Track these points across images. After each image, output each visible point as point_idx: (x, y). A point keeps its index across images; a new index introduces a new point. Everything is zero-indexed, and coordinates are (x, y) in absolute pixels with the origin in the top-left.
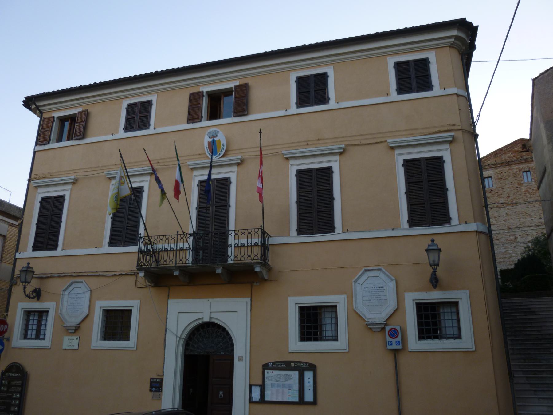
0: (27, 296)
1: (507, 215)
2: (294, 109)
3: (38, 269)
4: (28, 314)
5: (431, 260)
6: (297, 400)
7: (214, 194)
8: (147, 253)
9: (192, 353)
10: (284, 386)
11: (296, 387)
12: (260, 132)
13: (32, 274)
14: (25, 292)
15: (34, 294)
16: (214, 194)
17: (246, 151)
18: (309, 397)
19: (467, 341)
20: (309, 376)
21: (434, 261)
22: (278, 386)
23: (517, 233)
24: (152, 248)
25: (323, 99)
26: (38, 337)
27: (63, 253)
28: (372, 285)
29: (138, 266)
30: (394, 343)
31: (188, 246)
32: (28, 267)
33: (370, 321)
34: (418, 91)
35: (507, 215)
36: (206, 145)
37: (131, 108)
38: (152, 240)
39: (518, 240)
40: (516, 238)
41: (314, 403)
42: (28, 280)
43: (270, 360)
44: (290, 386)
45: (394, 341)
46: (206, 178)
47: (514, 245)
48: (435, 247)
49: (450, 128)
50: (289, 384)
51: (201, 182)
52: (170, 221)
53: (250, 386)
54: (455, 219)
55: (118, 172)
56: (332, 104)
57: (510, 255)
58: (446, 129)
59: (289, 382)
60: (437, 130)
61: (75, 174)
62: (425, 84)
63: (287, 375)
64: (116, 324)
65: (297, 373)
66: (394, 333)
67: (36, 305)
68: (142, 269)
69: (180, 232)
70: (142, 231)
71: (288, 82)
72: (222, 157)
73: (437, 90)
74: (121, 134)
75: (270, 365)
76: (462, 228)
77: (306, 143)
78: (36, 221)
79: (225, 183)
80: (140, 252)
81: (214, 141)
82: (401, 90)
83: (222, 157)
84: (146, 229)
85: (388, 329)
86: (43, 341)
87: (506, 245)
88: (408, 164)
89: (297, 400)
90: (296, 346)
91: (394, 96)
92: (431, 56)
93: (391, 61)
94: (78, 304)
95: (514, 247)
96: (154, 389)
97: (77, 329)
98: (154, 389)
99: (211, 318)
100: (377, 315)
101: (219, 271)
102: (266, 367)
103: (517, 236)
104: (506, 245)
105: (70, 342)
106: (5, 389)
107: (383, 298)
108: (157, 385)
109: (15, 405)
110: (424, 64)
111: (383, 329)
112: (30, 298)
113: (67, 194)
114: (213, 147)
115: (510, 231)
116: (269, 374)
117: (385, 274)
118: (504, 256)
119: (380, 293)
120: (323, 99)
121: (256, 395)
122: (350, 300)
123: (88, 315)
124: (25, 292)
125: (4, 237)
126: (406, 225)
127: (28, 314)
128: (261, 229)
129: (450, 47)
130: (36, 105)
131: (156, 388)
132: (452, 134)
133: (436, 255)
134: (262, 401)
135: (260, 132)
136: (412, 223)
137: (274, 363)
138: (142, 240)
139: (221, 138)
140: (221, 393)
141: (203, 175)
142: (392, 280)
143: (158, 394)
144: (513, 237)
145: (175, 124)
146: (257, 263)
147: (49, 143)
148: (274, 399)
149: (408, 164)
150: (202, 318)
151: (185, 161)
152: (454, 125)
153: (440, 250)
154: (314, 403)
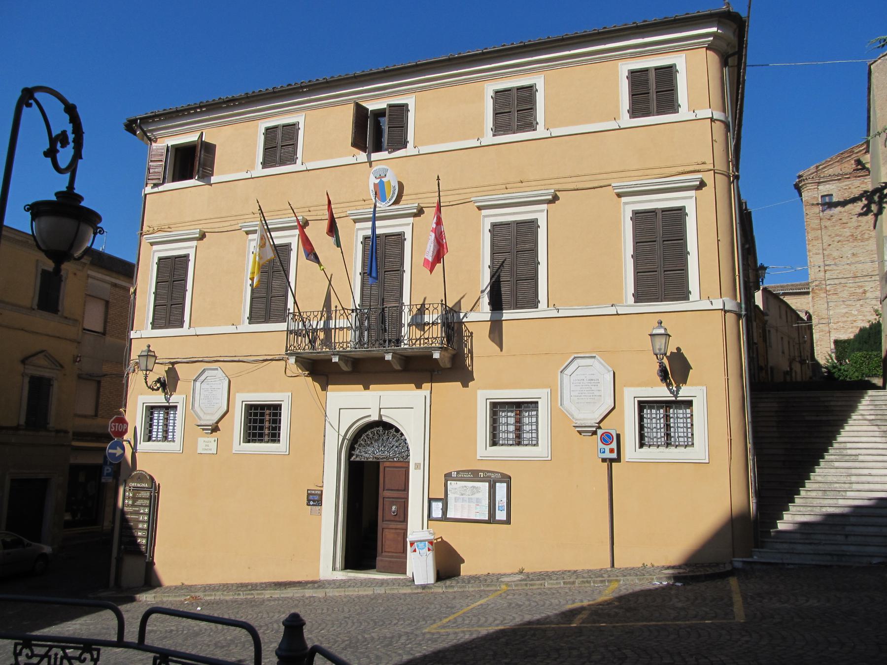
0: (149, 388)
1: (853, 255)
2: (489, 138)
3: (164, 352)
4: (151, 410)
5: (657, 347)
6: (115, 639)
7: (382, 256)
8: (297, 333)
9: (358, 459)
10: (470, 500)
11: (486, 502)
12: (438, 179)
13: (153, 359)
14: (146, 383)
15: (158, 385)
16: (382, 256)
17: (425, 196)
18: (501, 515)
19: (699, 451)
20: (501, 489)
21: (660, 349)
22: (463, 500)
23: (867, 283)
24: (304, 325)
25: (529, 124)
26: (165, 438)
27: (192, 331)
28: (583, 377)
29: (287, 350)
30: (607, 451)
31: (349, 325)
32: (149, 351)
33: (579, 423)
34: (660, 112)
35: (853, 255)
36: (372, 187)
37: (270, 132)
38: (305, 316)
39: (868, 295)
40: (865, 292)
41: (508, 521)
42: (150, 367)
43: (453, 469)
44: (478, 501)
45: (607, 448)
46: (369, 233)
47: (861, 302)
48: (662, 331)
49: (697, 168)
50: (477, 499)
51: (366, 238)
52: (327, 286)
53: (430, 500)
54: (694, 295)
55: (256, 223)
56: (541, 131)
57: (854, 318)
58: (691, 168)
59: (477, 496)
60: (681, 169)
61: (200, 227)
62: (667, 101)
63: (474, 487)
64: (262, 422)
65: (486, 485)
66: (606, 438)
67: (158, 398)
68: (291, 355)
69: (339, 308)
70: (290, 305)
71: (481, 97)
72: (393, 204)
73: (684, 113)
74: (259, 171)
75: (454, 475)
76: (705, 305)
77: (504, 186)
78: (153, 290)
79: (398, 239)
80: (289, 332)
81: (382, 182)
82: (635, 112)
83: (393, 204)
84: (295, 302)
85: (600, 432)
86: (172, 443)
87: (849, 303)
88: (638, 216)
89: (115, 639)
90: (485, 454)
91: (626, 120)
92: (679, 60)
93: (625, 67)
94: (209, 396)
95: (862, 306)
96: (312, 503)
97: (215, 429)
98: (312, 503)
99: (380, 416)
100: (590, 416)
101: (388, 357)
102: (448, 477)
103: (866, 289)
104: (849, 303)
105: (207, 444)
106: (130, 502)
107: (597, 393)
108: (316, 498)
109: (143, 522)
110: (667, 74)
111: (595, 433)
112: (153, 389)
113: (192, 253)
114: (380, 191)
115: (857, 280)
116: (452, 485)
117: (600, 363)
118: (845, 319)
119: (593, 388)
120: (529, 124)
121: (437, 512)
122: (556, 396)
123: (227, 411)
124: (146, 383)
125: (107, 302)
126: (631, 300)
127: (151, 410)
128: (442, 304)
129: (707, 48)
130: (142, 130)
131: (314, 501)
132: (699, 175)
133: (663, 340)
134: (444, 518)
135: (438, 179)
136: (639, 297)
137: (458, 472)
138: (291, 316)
139: (392, 180)
140: (394, 508)
141: (365, 229)
142: (609, 371)
143: (318, 508)
144: (861, 290)
145: (331, 157)
146: (436, 349)
147: (163, 183)
148: (458, 516)
149: (638, 216)
150: (370, 416)
151: (344, 210)
152: (704, 163)
153: (670, 336)
154: (508, 521)
